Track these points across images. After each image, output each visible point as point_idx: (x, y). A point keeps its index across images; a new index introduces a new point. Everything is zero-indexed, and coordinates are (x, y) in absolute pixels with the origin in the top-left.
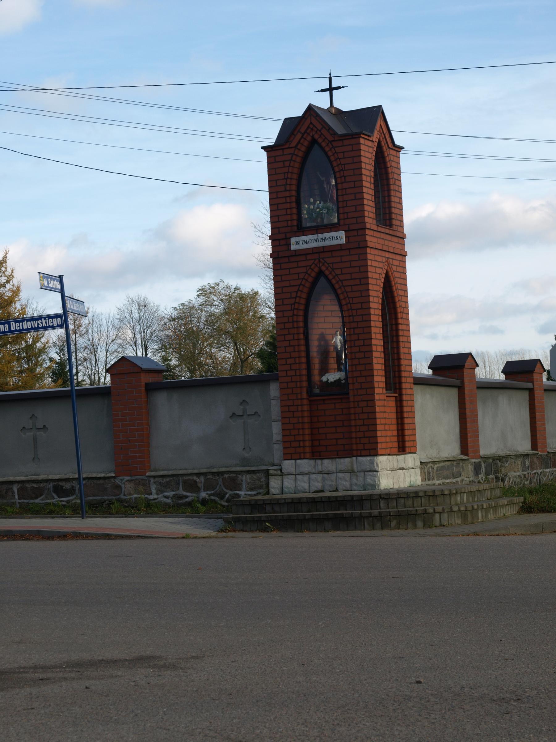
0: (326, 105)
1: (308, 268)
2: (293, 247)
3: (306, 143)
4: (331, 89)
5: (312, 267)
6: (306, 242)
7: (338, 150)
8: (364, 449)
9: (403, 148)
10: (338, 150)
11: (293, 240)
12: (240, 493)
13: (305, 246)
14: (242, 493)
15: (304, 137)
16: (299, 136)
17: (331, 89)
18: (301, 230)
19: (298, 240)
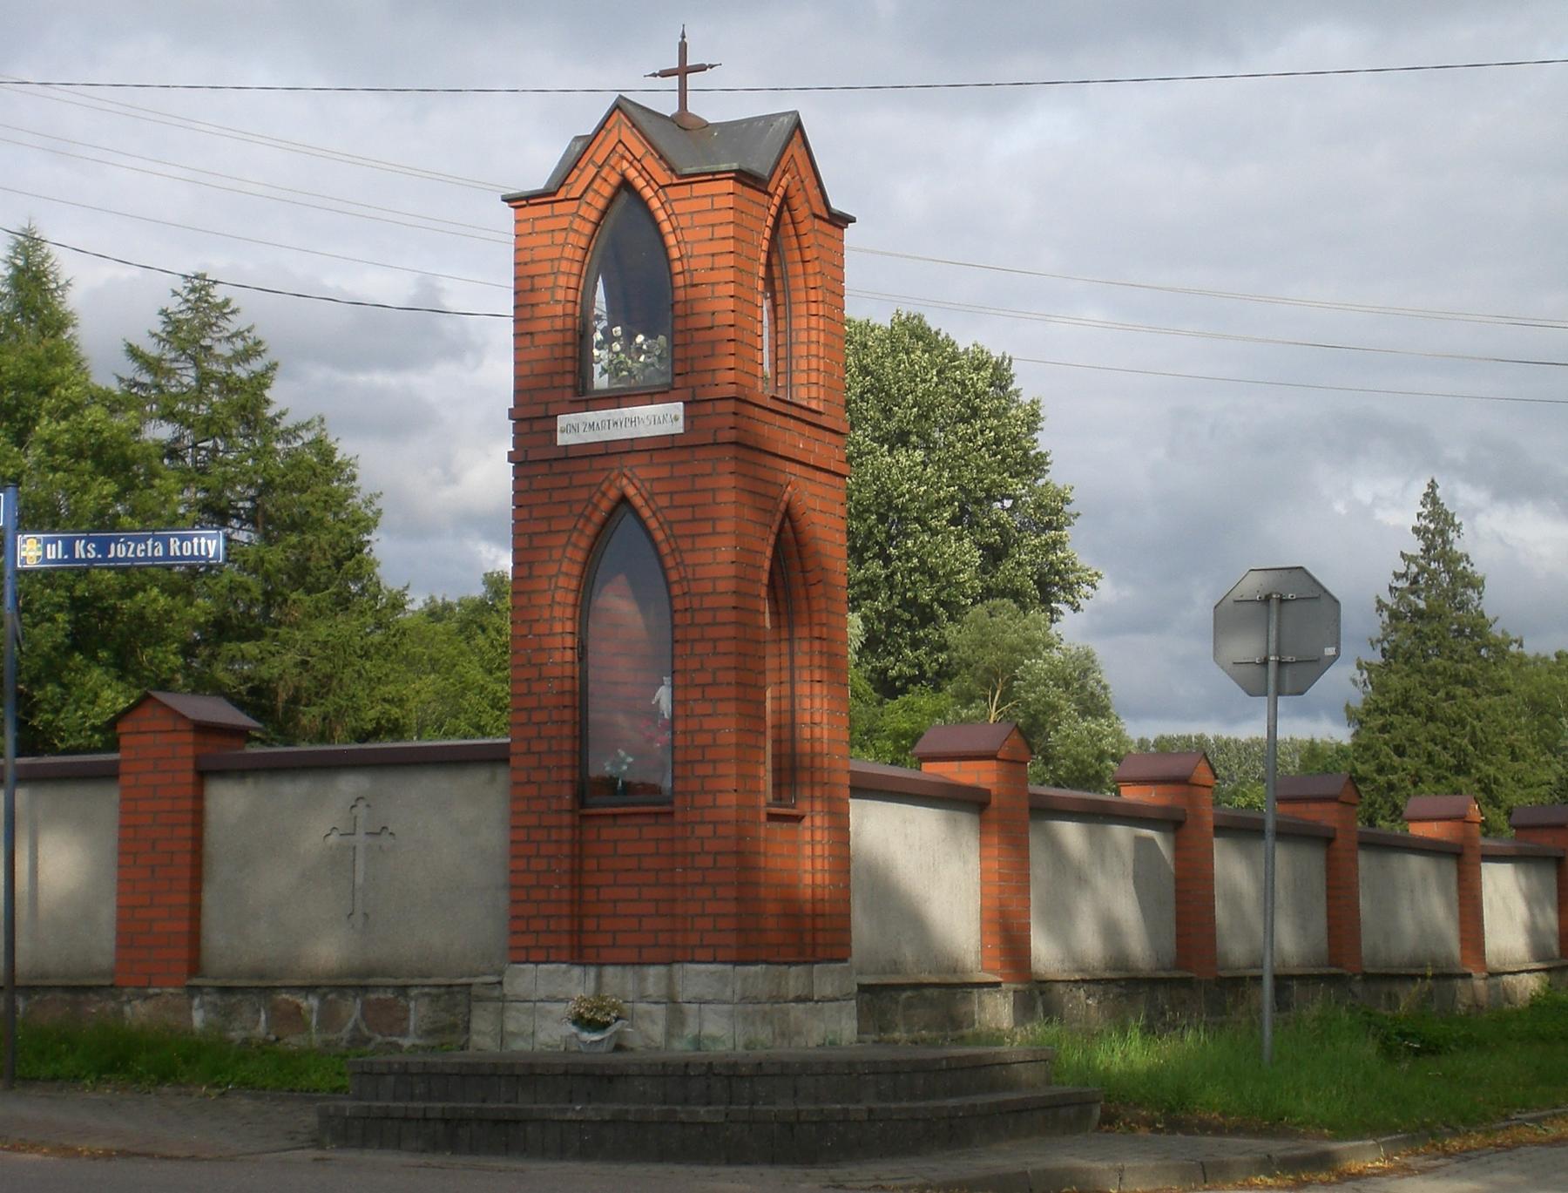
0: (669, 107)
1: (594, 489)
2: (563, 439)
3: (607, 191)
4: (683, 71)
5: (604, 487)
6: (592, 426)
7: (678, 207)
8: (702, 946)
9: (853, 220)
10: (678, 207)
11: (563, 420)
12: (401, 1041)
13: (591, 437)
14: (406, 1042)
15: (603, 174)
16: (591, 171)
17: (683, 71)
18: (586, 399)
19: (574, 422)
